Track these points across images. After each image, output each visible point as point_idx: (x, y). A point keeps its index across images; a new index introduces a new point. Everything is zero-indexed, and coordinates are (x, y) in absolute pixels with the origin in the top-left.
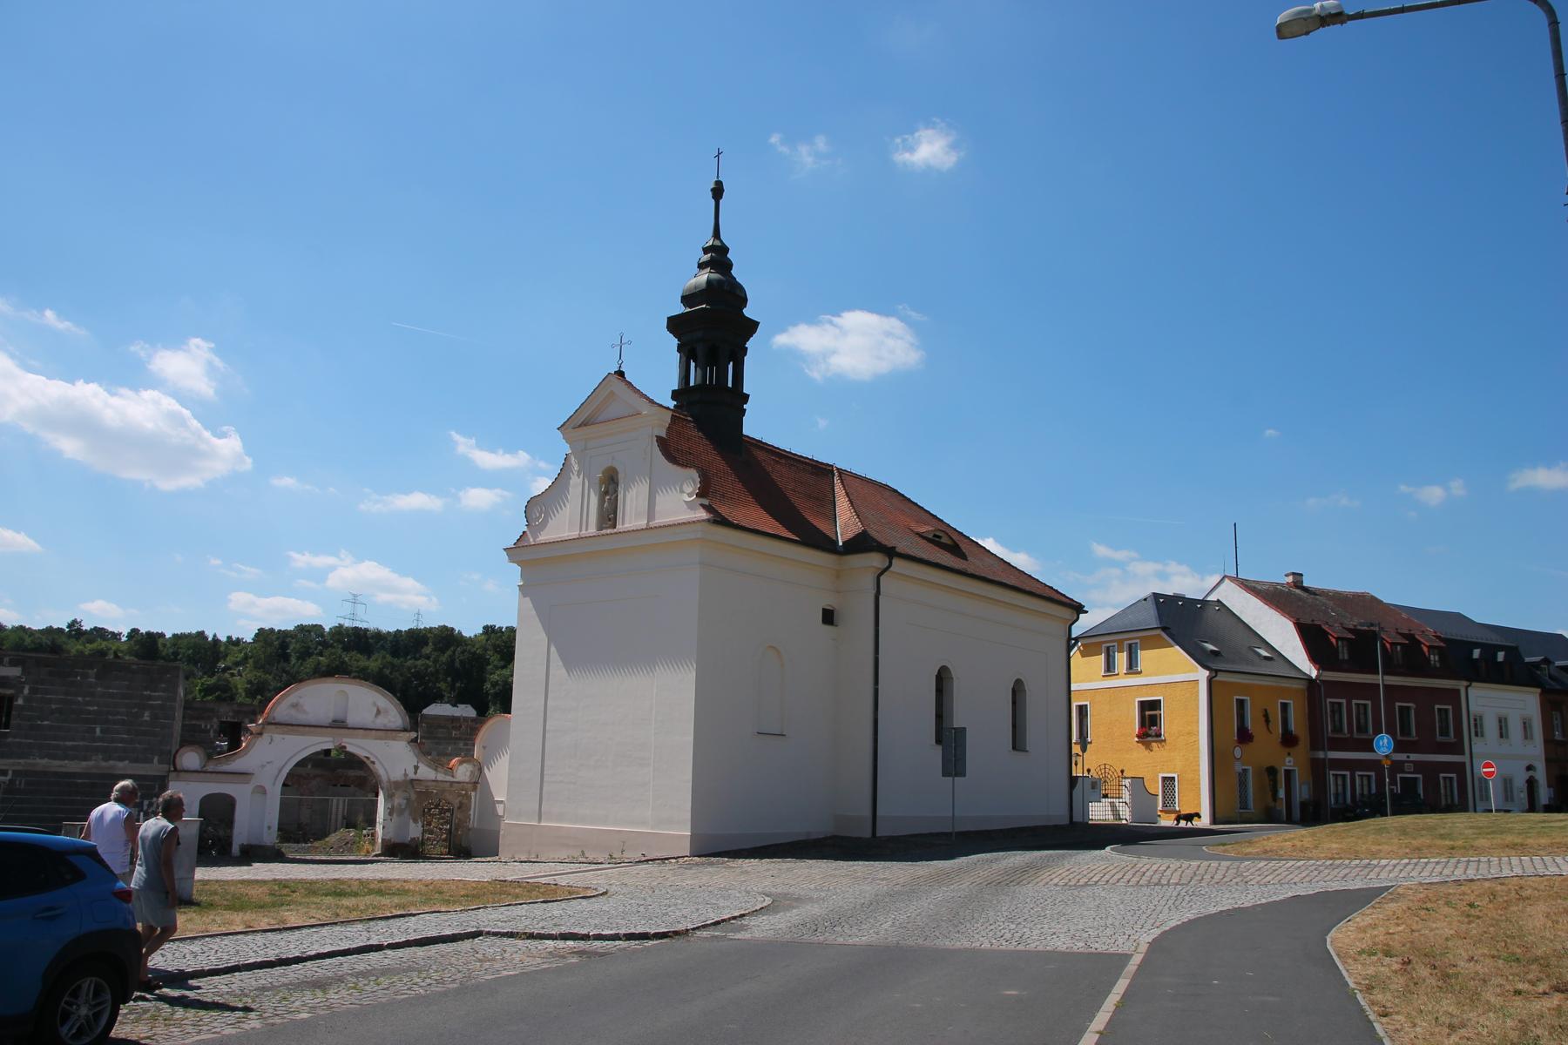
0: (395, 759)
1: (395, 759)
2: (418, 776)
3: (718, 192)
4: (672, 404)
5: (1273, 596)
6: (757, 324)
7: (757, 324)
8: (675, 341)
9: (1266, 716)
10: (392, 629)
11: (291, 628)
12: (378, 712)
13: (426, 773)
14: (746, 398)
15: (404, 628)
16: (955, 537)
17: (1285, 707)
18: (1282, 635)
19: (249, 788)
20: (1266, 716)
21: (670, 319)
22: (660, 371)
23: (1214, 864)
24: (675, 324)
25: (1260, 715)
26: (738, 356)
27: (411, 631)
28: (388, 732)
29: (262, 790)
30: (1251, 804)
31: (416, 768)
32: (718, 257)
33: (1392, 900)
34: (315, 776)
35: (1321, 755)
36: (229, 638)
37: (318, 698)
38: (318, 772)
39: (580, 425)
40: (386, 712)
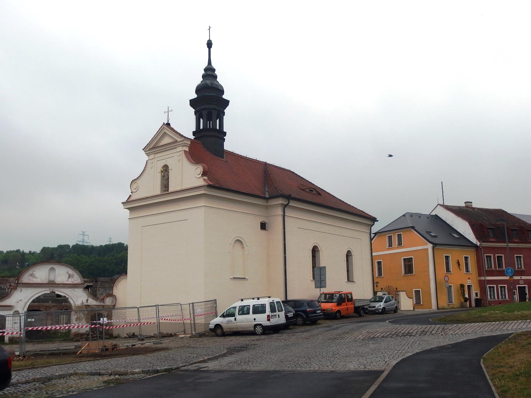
0: (78, 298)
1: (78, 298)
2: (89, 303)
3: (209, 45)
4: (192, 137)
5: (459, 211)
6: (228, 101)
7: (228, 101)
8: (193, 110)
9: (458, 263)
10: (98, 245)
11: (56, 246)
12: (69, 277)
13: (92, 302)
14: (225, 134)
15: (103, 244)
16: (319, 191)
17: (466, 258)
18: (463, 227)
19: (11, 312)
20: (458, 263)
21: (191, 101)
22: (186, 123)
23: (434, 326)
24: (193, 103)
25: (456, 261)
26: (221, 115)
27: (106, 246)
28: (74, 286)
29: (17, 313)
30: (454, 301)
31: (87, 300)
32: (210, 73)
33: (18, 361)
34: (53, 306)
35: (483, 278)
36: (30, 252)
37: (41, 274)
38: (54, 304)
39: (153, 148)
40: (73, 276)
